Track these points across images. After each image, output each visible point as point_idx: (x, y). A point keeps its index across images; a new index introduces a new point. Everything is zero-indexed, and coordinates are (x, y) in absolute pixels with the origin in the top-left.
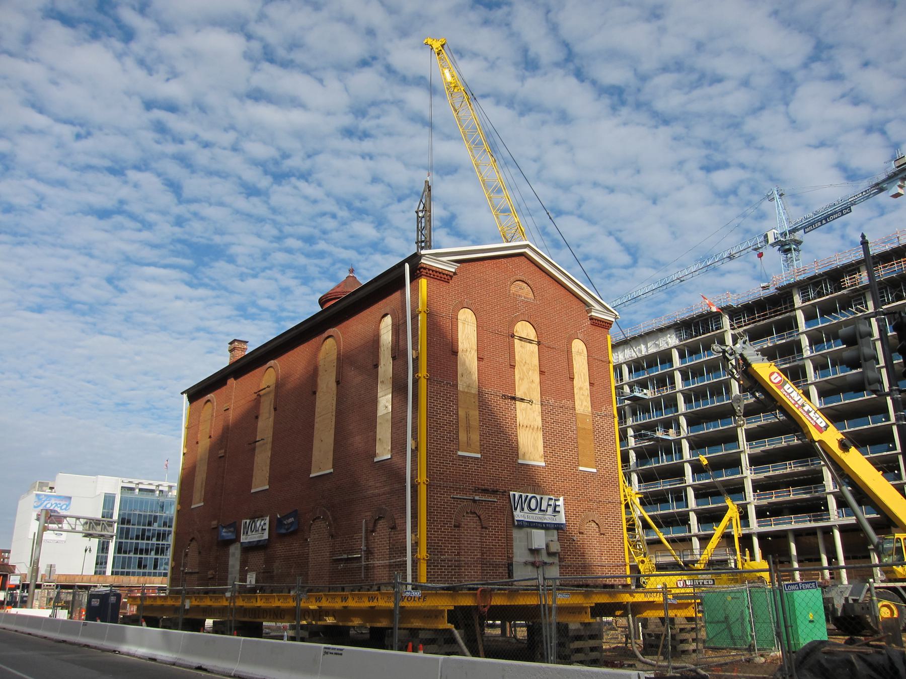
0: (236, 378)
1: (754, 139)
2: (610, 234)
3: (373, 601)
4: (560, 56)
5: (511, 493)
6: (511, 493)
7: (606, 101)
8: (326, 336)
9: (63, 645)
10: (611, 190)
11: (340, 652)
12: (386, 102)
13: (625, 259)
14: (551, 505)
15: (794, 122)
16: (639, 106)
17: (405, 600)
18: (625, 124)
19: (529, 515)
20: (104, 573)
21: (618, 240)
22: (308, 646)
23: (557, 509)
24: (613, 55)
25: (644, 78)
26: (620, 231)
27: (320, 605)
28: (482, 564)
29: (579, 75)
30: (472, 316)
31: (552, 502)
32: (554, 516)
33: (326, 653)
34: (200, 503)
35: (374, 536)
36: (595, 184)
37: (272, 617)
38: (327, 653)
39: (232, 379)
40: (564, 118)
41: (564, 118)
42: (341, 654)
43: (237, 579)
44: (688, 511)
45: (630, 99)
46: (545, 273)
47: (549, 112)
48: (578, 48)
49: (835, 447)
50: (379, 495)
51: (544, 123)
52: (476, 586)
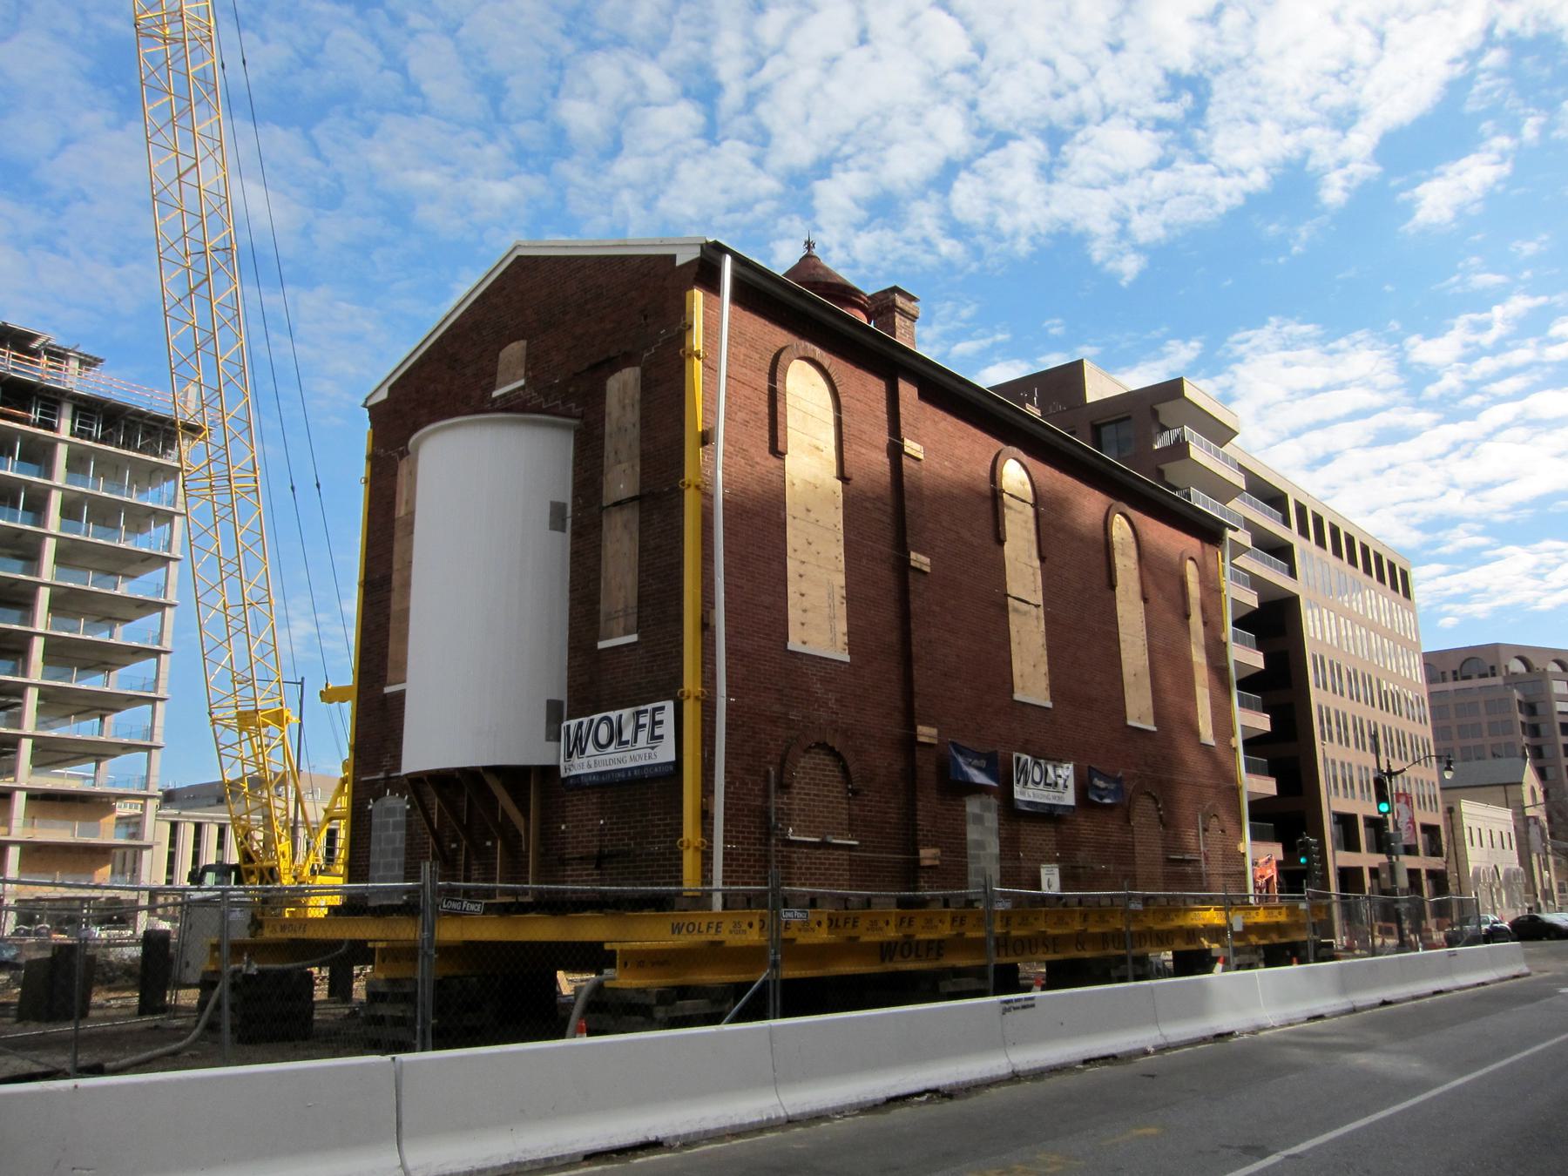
3: (679, 933)
5: (1015, 755)
6: (1015, 755)
8: (818, 358)
9: (900, 1114)
11: (1030, 1003)
12: (1278, 443)
14: (644, 726)
17: (684, 930)
22: (1100, 991)
23: (658, 732)
27: (910, 931)
31: (645, 720)
32: (653, 748)
33: (1005, 1011)
34: (627, 633)
37: (1116, 945)
38: (1007, 1010)
42: (1033, 1006)
43: (996, 876)
44: (27, 685)
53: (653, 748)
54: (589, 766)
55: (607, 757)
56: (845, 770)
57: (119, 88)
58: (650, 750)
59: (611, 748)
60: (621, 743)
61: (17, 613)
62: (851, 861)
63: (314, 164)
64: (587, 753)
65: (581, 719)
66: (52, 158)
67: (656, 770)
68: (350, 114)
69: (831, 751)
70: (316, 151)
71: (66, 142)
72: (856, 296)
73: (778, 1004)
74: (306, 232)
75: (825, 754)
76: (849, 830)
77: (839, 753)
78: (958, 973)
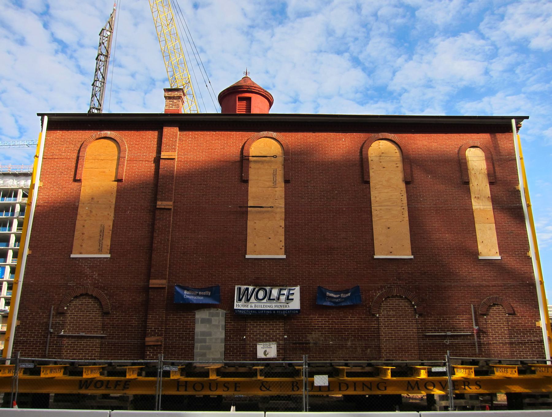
0: (181, 130)
1: (121, 102)
2: (13, 115)
4: (40, 9)
7: (55, 46)
8: (390, 138)
10: (29, 92)
13: (16, 133)
15: (145, 104)
16: (71, 57)
18: (60, 63)
19: (257, 304)
20: (473, 306)
21: (17, 121)
24: (69, 24)
25: (82, 46)
26: (20, 117)
28: (419, 351)
29: (46, 26)
30: (261, 153)
35: (486, 319)
36: (20, 85)
39: (178, 128)
40: (22, 42)
41: (22, 42)
45: (69, 52)
46: (281, 143)
47: (14, 33)
48: (52, 11)
49: (285, 297)
50: (489, 286)
51: (7, 37)
52: (59, 339)
53: (287, 303)
54: (251, 306)
55: (263, 304)
56: (101, 305)
57: (405, 45)
58: (286, 304)
59: (265, 301)
60: (269, 299)
61: (5, 244)
62: (102, 344)
63: (482, 42)
64: (251, 301)
65: (247, 287)
66: (392, 79)
67: (254, 312)
68: (493, 14)
69: (91, 296)
70: (482, 36)
71: (394, 73)
72: (240, 88)
73: (157, 404)
74: (487, 72)
75: (88, 298)
76: (102, 330)
77: (95, 297)
78: (93, 397)
